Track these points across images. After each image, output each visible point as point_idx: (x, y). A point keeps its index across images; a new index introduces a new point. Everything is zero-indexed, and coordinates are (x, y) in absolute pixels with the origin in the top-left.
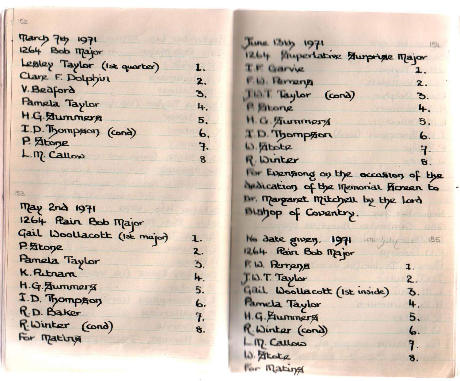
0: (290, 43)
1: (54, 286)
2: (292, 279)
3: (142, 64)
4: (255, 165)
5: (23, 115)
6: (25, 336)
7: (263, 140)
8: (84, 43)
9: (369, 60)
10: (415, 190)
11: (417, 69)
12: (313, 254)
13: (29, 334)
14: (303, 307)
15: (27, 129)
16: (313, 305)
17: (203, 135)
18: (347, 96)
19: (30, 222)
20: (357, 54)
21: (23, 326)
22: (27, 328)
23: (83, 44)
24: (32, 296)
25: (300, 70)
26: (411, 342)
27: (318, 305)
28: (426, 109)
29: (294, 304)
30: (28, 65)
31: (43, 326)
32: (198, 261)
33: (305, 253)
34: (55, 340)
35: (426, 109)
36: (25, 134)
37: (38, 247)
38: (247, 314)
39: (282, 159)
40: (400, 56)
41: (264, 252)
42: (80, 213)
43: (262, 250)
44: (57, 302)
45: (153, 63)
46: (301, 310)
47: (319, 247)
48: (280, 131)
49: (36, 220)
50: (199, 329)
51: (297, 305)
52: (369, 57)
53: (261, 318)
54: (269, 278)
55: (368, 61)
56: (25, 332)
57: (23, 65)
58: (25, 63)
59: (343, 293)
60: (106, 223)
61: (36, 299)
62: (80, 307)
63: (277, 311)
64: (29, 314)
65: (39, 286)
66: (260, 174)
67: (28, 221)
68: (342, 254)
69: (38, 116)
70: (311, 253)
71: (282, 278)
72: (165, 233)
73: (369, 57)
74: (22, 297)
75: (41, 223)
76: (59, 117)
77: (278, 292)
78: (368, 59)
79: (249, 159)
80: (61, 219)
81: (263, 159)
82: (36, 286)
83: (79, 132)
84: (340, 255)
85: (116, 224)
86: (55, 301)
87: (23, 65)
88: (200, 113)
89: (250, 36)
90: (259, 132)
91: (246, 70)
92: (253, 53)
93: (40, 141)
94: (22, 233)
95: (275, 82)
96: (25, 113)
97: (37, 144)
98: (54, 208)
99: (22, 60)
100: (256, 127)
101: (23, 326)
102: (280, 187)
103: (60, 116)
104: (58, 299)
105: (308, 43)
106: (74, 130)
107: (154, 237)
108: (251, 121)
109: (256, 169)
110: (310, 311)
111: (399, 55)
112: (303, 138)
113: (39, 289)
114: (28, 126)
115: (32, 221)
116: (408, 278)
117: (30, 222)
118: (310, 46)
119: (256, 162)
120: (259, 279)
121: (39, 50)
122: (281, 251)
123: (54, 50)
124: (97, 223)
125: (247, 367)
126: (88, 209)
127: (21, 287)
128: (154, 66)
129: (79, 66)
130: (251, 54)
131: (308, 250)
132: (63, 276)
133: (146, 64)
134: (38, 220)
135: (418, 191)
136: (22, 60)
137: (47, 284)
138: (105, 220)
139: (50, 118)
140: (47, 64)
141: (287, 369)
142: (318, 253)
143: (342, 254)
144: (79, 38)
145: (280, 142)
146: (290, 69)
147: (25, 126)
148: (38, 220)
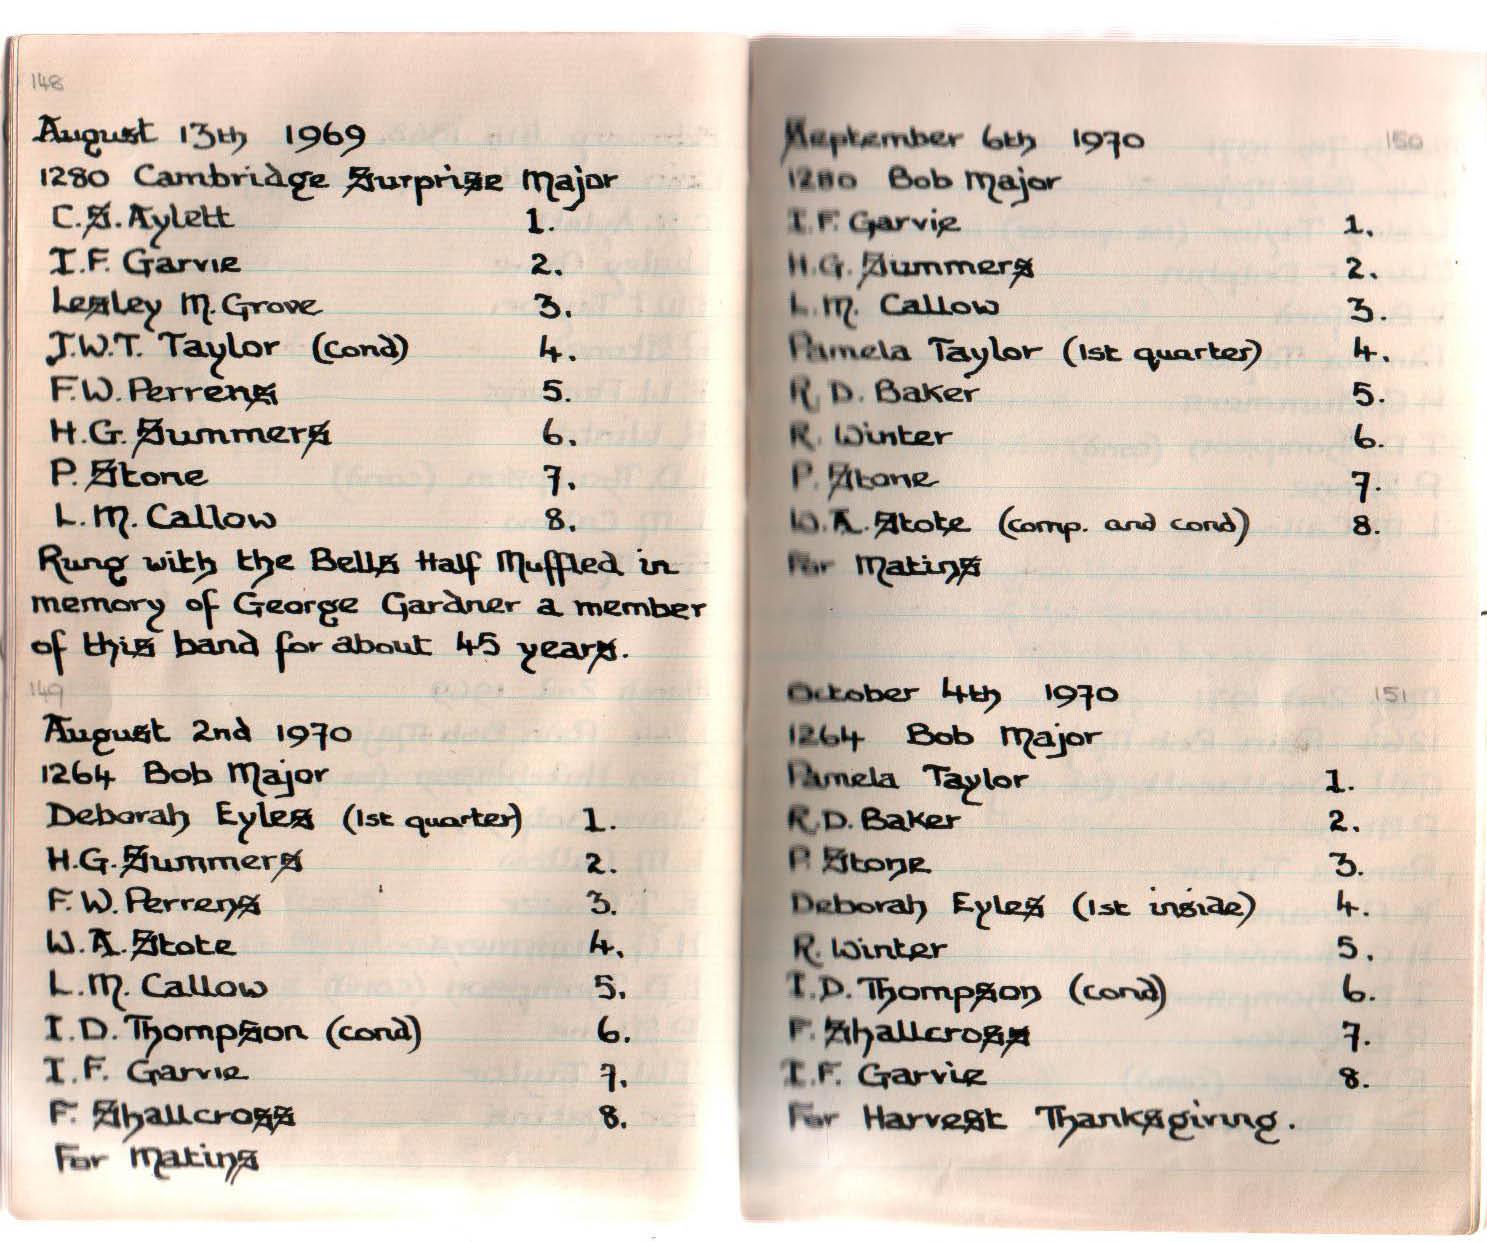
5: (56, 431)
19: (68, 782)
25: (943, 226)
26: (1350, 1030)
28: (1375, 354)
30: (73, 308)
35: (1375, 354)
37: (119, 475)
39: (902, 433)
41: (855, 739)
43: (849, 733)
44: (158, 1039)
45: (338, 1048)
48: (879, 981)
54: (135, 349)
57: (57, 308)
58: (65, 301)
62: (236, 1053)
65: (104, 861)
67: (64, 777)
68: (1056, 739)
69: (107, 433)
72: (513, 806)
75: (102, 782)
76: (180, 437)
81: (840, 947)
82: (95, 860)
84: (1050, 743)
85: (233, 779)
86: (153, 1035)
91: (790, 228)
92: (809, 174)
96: (62, 425)
101: (50, 566)
103: (186, 434)
104: (162, 1029)
108: (798, 270)
113: (102, 869)
115: (77, 777)
117: (68, 782)
120: (71, 950)
121: (855, 734)
124: (935, 738)
132: (212, 652)
134: (93, 774)
137: (131, 851)
139: (148, 437)
143: (1056, 739)
146: (915, 222)
147: (62, 253)
148: (93, 773)
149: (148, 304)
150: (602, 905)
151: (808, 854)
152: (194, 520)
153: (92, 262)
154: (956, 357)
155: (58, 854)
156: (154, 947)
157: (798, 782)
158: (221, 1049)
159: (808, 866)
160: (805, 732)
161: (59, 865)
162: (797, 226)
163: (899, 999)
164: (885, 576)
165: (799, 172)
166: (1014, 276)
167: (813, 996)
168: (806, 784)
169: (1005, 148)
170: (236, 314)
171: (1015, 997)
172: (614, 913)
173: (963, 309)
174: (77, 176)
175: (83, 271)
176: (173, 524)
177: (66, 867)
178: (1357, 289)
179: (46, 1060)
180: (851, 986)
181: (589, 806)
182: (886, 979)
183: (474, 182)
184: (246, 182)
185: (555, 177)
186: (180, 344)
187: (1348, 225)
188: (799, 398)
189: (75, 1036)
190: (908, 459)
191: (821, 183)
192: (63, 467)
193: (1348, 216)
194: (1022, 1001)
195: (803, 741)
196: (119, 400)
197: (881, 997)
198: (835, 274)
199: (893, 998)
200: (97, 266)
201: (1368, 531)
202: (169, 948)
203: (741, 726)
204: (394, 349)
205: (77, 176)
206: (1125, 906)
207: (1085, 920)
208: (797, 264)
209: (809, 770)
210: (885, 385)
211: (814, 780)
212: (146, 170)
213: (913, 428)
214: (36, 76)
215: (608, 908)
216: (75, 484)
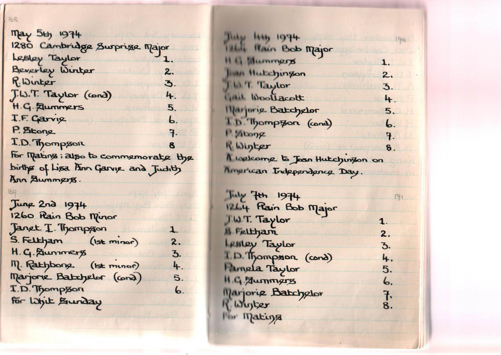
1: (45, 107)
2: (273, 220)
4: (231, 310)
7: (239, 128)
8: (66, 37)
12: (294, 210)
14: (282, 272)
15: (17, 118)
16: (292, 270)
17: (390, 126)
19: (20, 218)
22: (19, 85)
27: (296, 270)
29: (273, 269)
30: (19, 59)
31: (32, 83)
32: (387, 84)
33: (287, 209)
36: (15, 124)
38: (227, 278)
43: (295, 36)
46: (280, 273)
47: (301, 202)
49: (25, 216)
53: (240, 282)
54: (250, 220)
57: (14, 59)
58: (16, 57)
61: (26, 143)
63: (256, 275)
64: (20, 83)
66: (236, 318)
70: (293, 208)
71: (263, 220)
74: (14, 141)
78: (116, 48)
79: (228, 145)
80: (45, 214)
83: (64, 290)
87: (14, 59)
89: (230, 188)
90: (235, 254)
93: (27, 129)
95: (261, 37)
98: (44, 205)
99: (14, 54)
105: (281, 37)
106: (60, 289)
109: (233, 313)
110: (288, 275)
114: (17, 115)
116: (166, 71)
119: (231, 307)
122: (262, 206)
125: (225, 316)
126: (76, 206)
127: (14, 108)
130: (231, 206)
131: (277, 290)
136: (14, 54)
138: (52, 263)
140: (37, 59)
141: (265, 318)
142: (300, 208)
144: (66, 203)
147: (14, 116)
149: (39, 58)
150: (176, 254)
153: (23, 119)
154: (267, 209)
155: (15, 250)
156: (43, 107)
158: (62, 149)
161: (16, 107)
169: (291, 247)
170: (337, 161)
172: (180, 256)
174: (22, 45)
175: (19, 145)
176: (47, 47)
177: (18, 108)
179: (12, 115)
181: (172, 226)
183: (131, 48)
184: (70, 47)
185: (315, 48)
187: (383, 62)
189: (18, 132)
192: (16, 128)
193: (382, 59)
195: (231, 209)
196: (30, 145)
198: (265, 72)
200: (24, 119)
201: (388, 307)
202: (43, 156)
204: (108, 95)
205: (22, 45)
206: (104, 242)
207: (93, 269)
209: (232, 266)
210: (285, 47)
212: (35, 117)
214: (10, 17)
215: (178, 256)
216: (19, 133)
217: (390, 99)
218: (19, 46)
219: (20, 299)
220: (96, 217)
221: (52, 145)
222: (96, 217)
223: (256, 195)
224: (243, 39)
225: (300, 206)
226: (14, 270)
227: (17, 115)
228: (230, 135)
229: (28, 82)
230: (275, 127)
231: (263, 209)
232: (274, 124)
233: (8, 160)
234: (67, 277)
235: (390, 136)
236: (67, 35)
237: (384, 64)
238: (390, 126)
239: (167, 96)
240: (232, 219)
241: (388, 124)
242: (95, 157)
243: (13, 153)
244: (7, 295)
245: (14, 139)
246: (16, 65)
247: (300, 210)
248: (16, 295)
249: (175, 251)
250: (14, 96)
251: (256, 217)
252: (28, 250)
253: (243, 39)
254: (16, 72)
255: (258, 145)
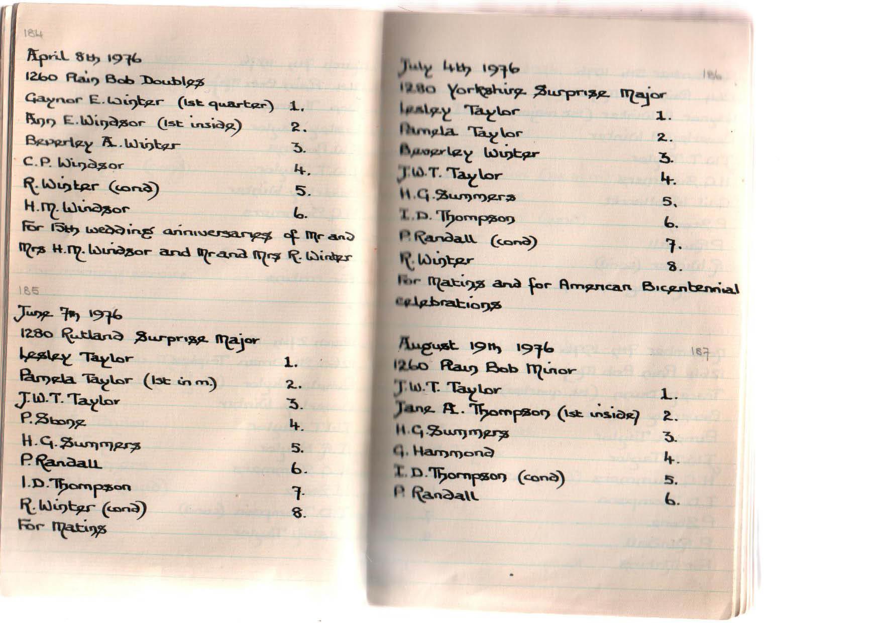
0: (464, 68)
3: (245, 101)
6: (26, 523)
9: (570, 97)
10: (154, 105)
11: (659, 114)
13: (35, 521)
17: (670, 225)
18: (554, 477)
20: (550, 87)
21: (25, 507)
22: (32, 511)
23: (77, 514)
24: (146, 77)
34: (73, 530)
35: (305, 171)
40: (624, 92)
42: (133, 109)
50: (297, 513)
51: (96, 359)
52: (570, 93)
55: (568, 99)
56: (27, 516)
57: (22, 356)
59: (154, 382)
60: (130, 82)
73: (570, 93)
77: (45, 185)
88: (299, 179)
92: (411, 86)
94: (31, 97)
97: (38, 422)
100: (415, 205)
102: (461, 305)
105: (489, 68)
107: (239, 341)
108: (406, 197)
111: (622, 91)
112: (478, 221)
118: (492, 72)
123: (110, 78)
126: (501, 69)
127: (26, 209)
128: (265, 105)
129: (99, 403)
130: (408, 87)
133: (252, 101)
135: (626, 291)
145: (449, 229)
151: (403, 490)
152: (87, 465)
155: (29, 203)
157: (404, 132)
158: (515, 421)
159: (404, 496)
160: (402, 364)
162: (404, 217)
163: (448, 479)
164: (441, 287)
165: (399, 362)
166: (500, 438)
167: (413, 219)
168: (408, 132)
171: (504, 221)
173: (476, 306)
178: (663, 147)
180: (425, 471)
182: (443, 469)
186: (91, 356)
187: (658, 115)
188: (405, 262)
190: (455, 251)
191: (419, 90)
194: (507, 222)
197: (448, 219)
199: (445, 478)
203: (373, 245)
208: (400, 430)
211: (411, 130)
213: (454, 255)
217: (670, 178)
218: (33, 334)
219: (36, 225)
220: (26, 249)
221: (466, 219)
222: (26, 249)
223: (66, 314)
224: (428, 70)
225: (512, 366)
226: (23, 514)
227: (29, 393)
228: (405, 239)
229: (52, 185)
230: (480, 224)
231: (449, 369)
232: (480, 220)
233: (18, 235)
234: (83, 400)
235: (673, 244)
236: (121, 58)
237: (661, 118)
238: (670, 225)
239: (296, 170)
240: (409, 172)
241: (669, 498)
242: (130, 82)
243: (26, 224)
244: (13, 513)
245: (25, 394)
246: (33, 134)
247: (511, 371)
248: (29, 215)
249: (669, 433)
250: (22, 315)
251: (448, 383)
252: (48, 437)
253: (428, 70)
254: (32, 144)
255: (453, 259)
